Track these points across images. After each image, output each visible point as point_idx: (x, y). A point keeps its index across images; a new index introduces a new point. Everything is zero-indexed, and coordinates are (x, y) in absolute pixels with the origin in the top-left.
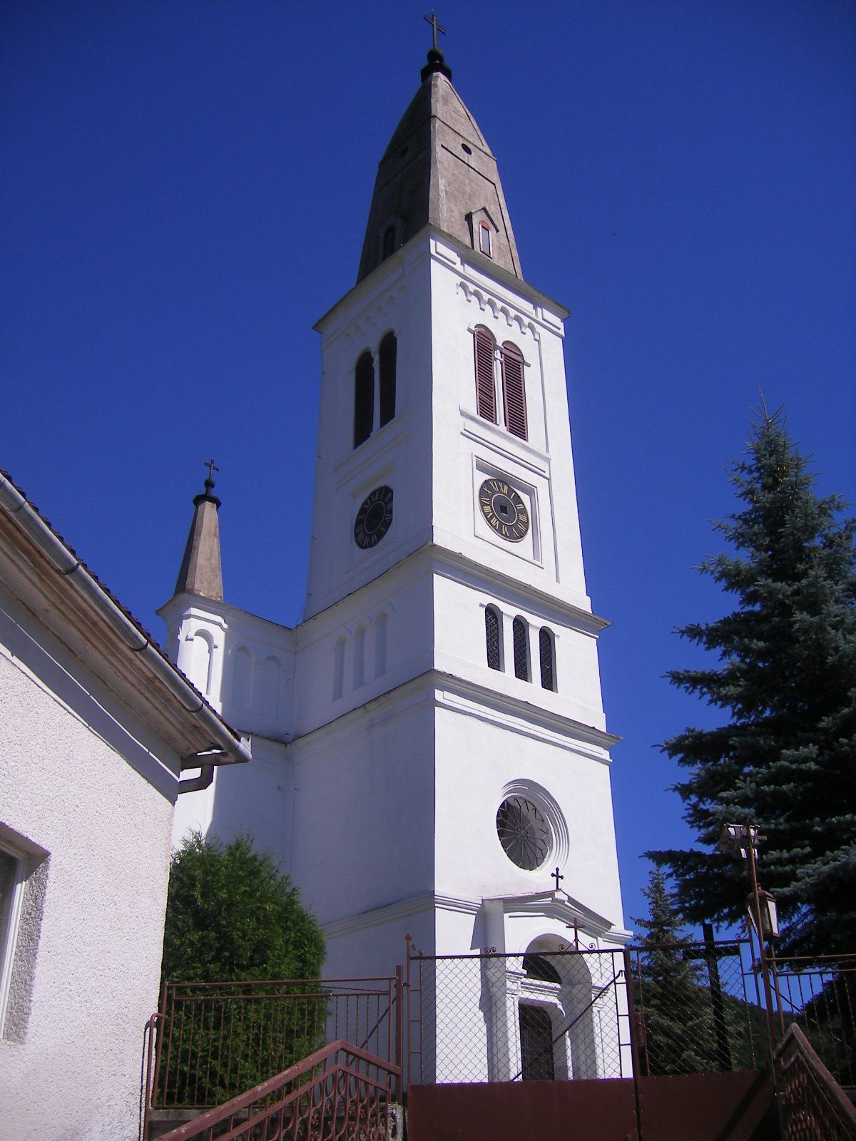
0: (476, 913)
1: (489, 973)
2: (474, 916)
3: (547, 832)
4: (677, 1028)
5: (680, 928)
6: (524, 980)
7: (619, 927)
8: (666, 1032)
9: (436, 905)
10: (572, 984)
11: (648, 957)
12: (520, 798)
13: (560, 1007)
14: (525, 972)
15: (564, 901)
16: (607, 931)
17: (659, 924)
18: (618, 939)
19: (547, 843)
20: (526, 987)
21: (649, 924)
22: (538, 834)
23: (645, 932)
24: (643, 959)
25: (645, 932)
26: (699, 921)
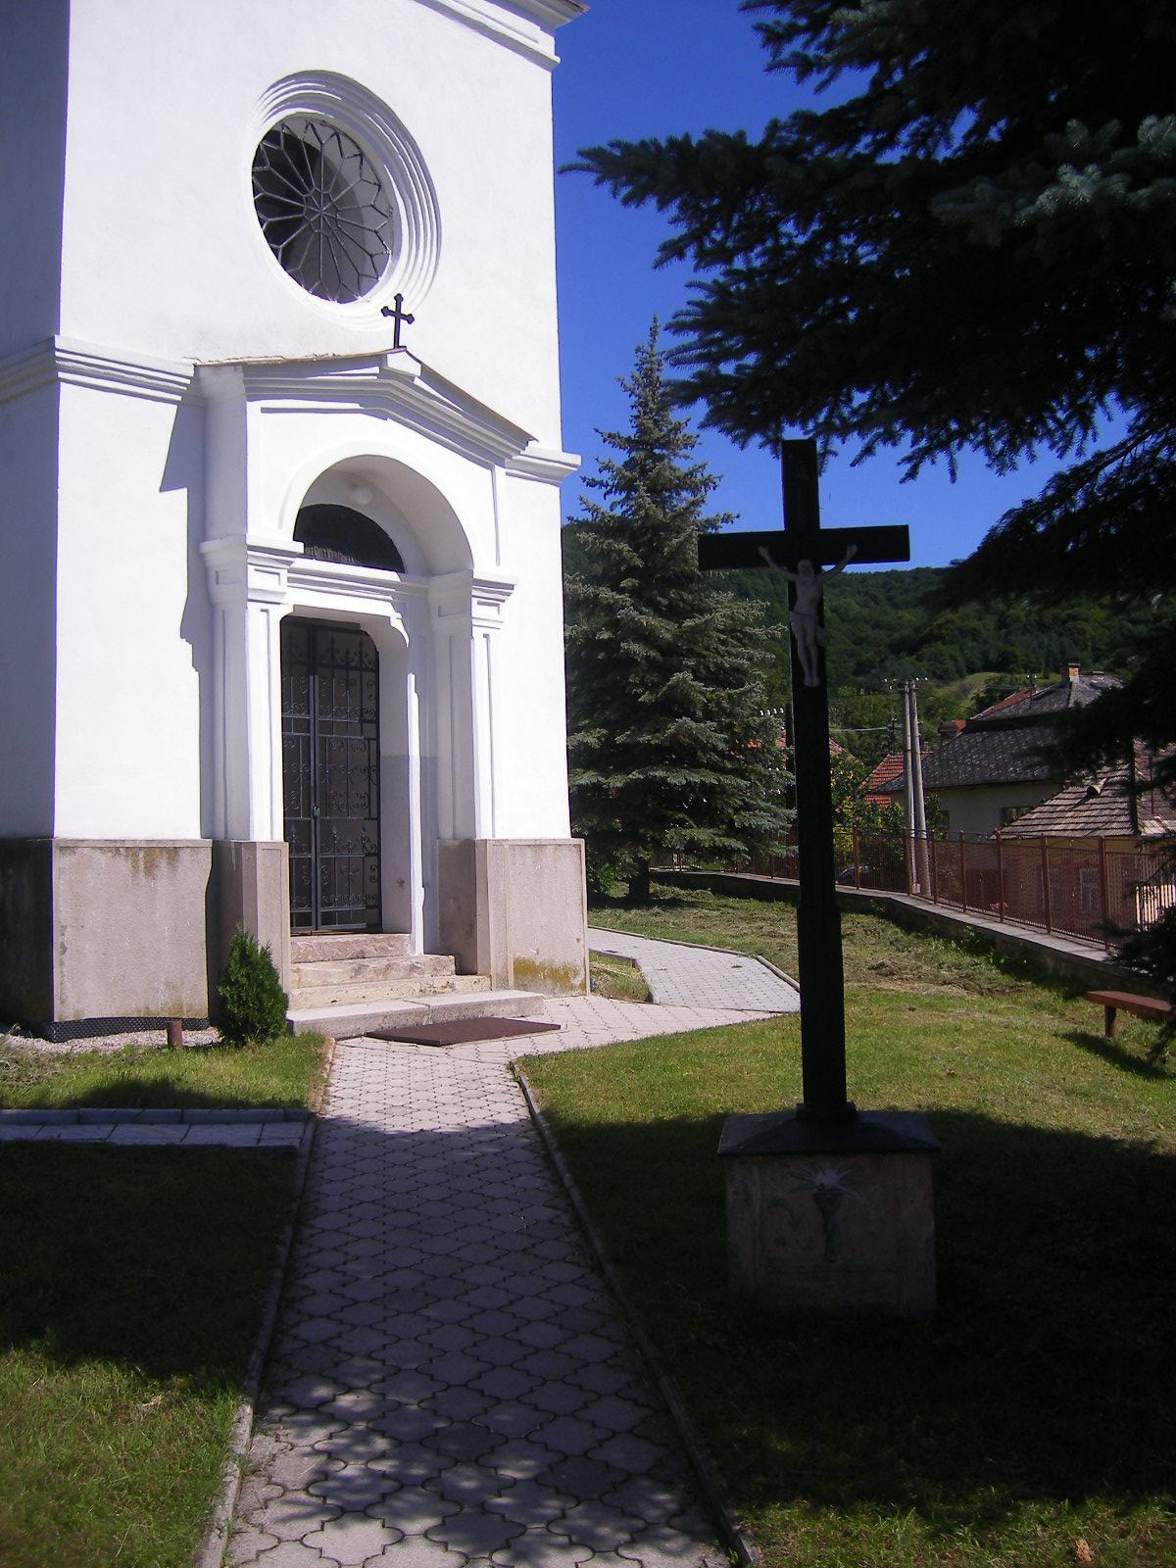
0: (179, 398)
1: (207, 547)
2: (175, 407)
3: (389, 214)
4: (666, 630)
5: (684, 452)
6: (301, 563)
7: (547, 442)
8: (646, 637)
9: (61, 375)
10: (429, 572)
11: (622, 503)
12: (324, 123)
13: (397, 623)
14: (299, 547)
15: (412, 378)
16: (519, 454)
17: (647, 443)
18: (546, 472)
19: (388, 242)
20: (299, 579)
21: (630, 444)
22: (371, 220)
23: (619, 457)
24: (610, 505)
25: (619, 457)
26: (764, 434)
